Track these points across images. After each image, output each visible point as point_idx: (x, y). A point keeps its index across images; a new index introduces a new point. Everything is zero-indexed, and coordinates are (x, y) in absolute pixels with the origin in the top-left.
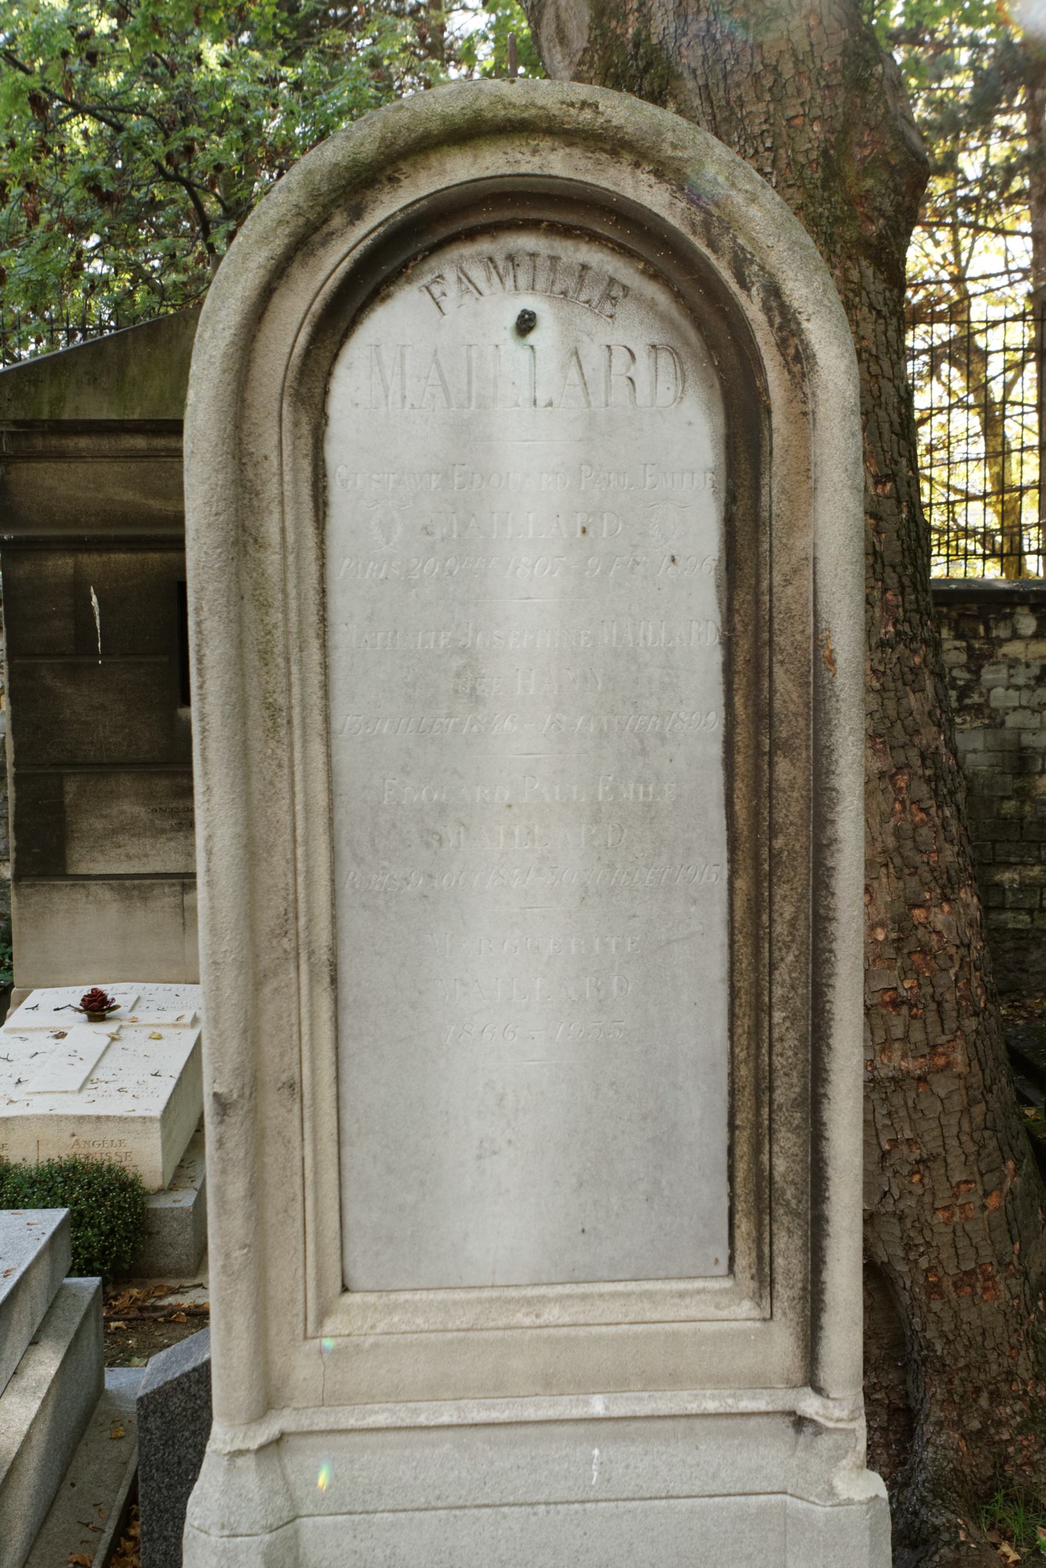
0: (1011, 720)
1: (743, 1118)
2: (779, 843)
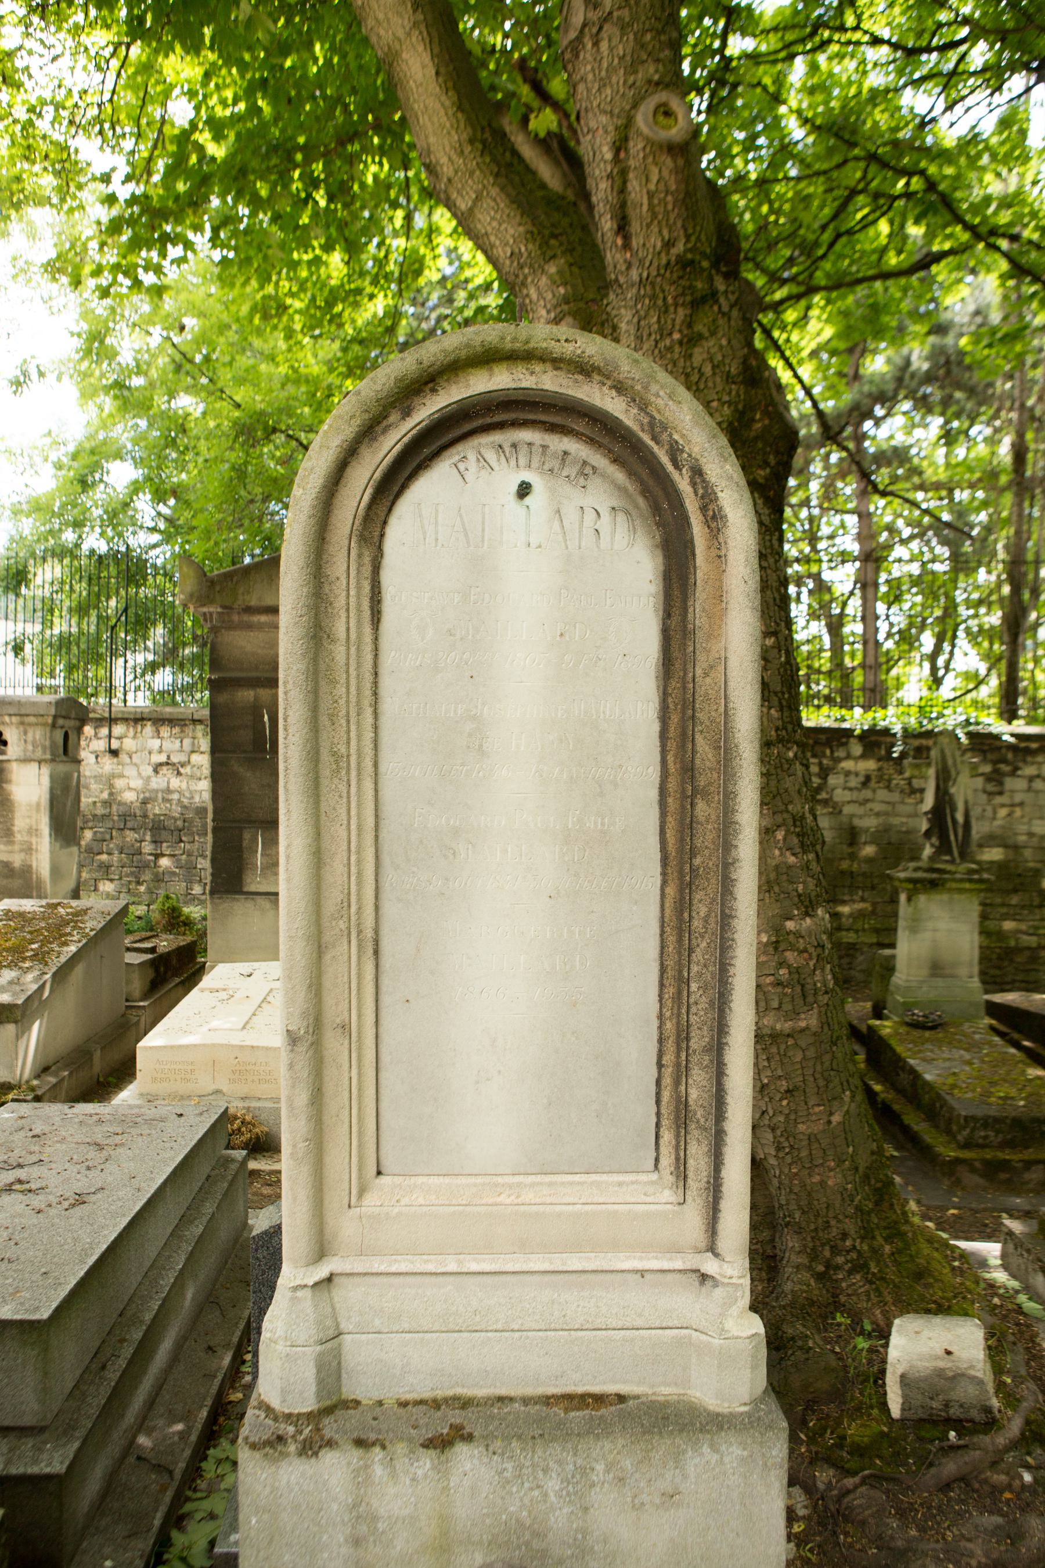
0: (847, 810)
1: (669, 1058)
2: (697, 861)
